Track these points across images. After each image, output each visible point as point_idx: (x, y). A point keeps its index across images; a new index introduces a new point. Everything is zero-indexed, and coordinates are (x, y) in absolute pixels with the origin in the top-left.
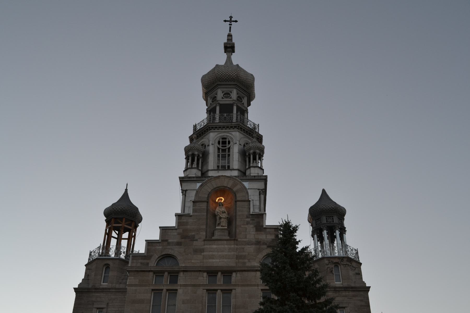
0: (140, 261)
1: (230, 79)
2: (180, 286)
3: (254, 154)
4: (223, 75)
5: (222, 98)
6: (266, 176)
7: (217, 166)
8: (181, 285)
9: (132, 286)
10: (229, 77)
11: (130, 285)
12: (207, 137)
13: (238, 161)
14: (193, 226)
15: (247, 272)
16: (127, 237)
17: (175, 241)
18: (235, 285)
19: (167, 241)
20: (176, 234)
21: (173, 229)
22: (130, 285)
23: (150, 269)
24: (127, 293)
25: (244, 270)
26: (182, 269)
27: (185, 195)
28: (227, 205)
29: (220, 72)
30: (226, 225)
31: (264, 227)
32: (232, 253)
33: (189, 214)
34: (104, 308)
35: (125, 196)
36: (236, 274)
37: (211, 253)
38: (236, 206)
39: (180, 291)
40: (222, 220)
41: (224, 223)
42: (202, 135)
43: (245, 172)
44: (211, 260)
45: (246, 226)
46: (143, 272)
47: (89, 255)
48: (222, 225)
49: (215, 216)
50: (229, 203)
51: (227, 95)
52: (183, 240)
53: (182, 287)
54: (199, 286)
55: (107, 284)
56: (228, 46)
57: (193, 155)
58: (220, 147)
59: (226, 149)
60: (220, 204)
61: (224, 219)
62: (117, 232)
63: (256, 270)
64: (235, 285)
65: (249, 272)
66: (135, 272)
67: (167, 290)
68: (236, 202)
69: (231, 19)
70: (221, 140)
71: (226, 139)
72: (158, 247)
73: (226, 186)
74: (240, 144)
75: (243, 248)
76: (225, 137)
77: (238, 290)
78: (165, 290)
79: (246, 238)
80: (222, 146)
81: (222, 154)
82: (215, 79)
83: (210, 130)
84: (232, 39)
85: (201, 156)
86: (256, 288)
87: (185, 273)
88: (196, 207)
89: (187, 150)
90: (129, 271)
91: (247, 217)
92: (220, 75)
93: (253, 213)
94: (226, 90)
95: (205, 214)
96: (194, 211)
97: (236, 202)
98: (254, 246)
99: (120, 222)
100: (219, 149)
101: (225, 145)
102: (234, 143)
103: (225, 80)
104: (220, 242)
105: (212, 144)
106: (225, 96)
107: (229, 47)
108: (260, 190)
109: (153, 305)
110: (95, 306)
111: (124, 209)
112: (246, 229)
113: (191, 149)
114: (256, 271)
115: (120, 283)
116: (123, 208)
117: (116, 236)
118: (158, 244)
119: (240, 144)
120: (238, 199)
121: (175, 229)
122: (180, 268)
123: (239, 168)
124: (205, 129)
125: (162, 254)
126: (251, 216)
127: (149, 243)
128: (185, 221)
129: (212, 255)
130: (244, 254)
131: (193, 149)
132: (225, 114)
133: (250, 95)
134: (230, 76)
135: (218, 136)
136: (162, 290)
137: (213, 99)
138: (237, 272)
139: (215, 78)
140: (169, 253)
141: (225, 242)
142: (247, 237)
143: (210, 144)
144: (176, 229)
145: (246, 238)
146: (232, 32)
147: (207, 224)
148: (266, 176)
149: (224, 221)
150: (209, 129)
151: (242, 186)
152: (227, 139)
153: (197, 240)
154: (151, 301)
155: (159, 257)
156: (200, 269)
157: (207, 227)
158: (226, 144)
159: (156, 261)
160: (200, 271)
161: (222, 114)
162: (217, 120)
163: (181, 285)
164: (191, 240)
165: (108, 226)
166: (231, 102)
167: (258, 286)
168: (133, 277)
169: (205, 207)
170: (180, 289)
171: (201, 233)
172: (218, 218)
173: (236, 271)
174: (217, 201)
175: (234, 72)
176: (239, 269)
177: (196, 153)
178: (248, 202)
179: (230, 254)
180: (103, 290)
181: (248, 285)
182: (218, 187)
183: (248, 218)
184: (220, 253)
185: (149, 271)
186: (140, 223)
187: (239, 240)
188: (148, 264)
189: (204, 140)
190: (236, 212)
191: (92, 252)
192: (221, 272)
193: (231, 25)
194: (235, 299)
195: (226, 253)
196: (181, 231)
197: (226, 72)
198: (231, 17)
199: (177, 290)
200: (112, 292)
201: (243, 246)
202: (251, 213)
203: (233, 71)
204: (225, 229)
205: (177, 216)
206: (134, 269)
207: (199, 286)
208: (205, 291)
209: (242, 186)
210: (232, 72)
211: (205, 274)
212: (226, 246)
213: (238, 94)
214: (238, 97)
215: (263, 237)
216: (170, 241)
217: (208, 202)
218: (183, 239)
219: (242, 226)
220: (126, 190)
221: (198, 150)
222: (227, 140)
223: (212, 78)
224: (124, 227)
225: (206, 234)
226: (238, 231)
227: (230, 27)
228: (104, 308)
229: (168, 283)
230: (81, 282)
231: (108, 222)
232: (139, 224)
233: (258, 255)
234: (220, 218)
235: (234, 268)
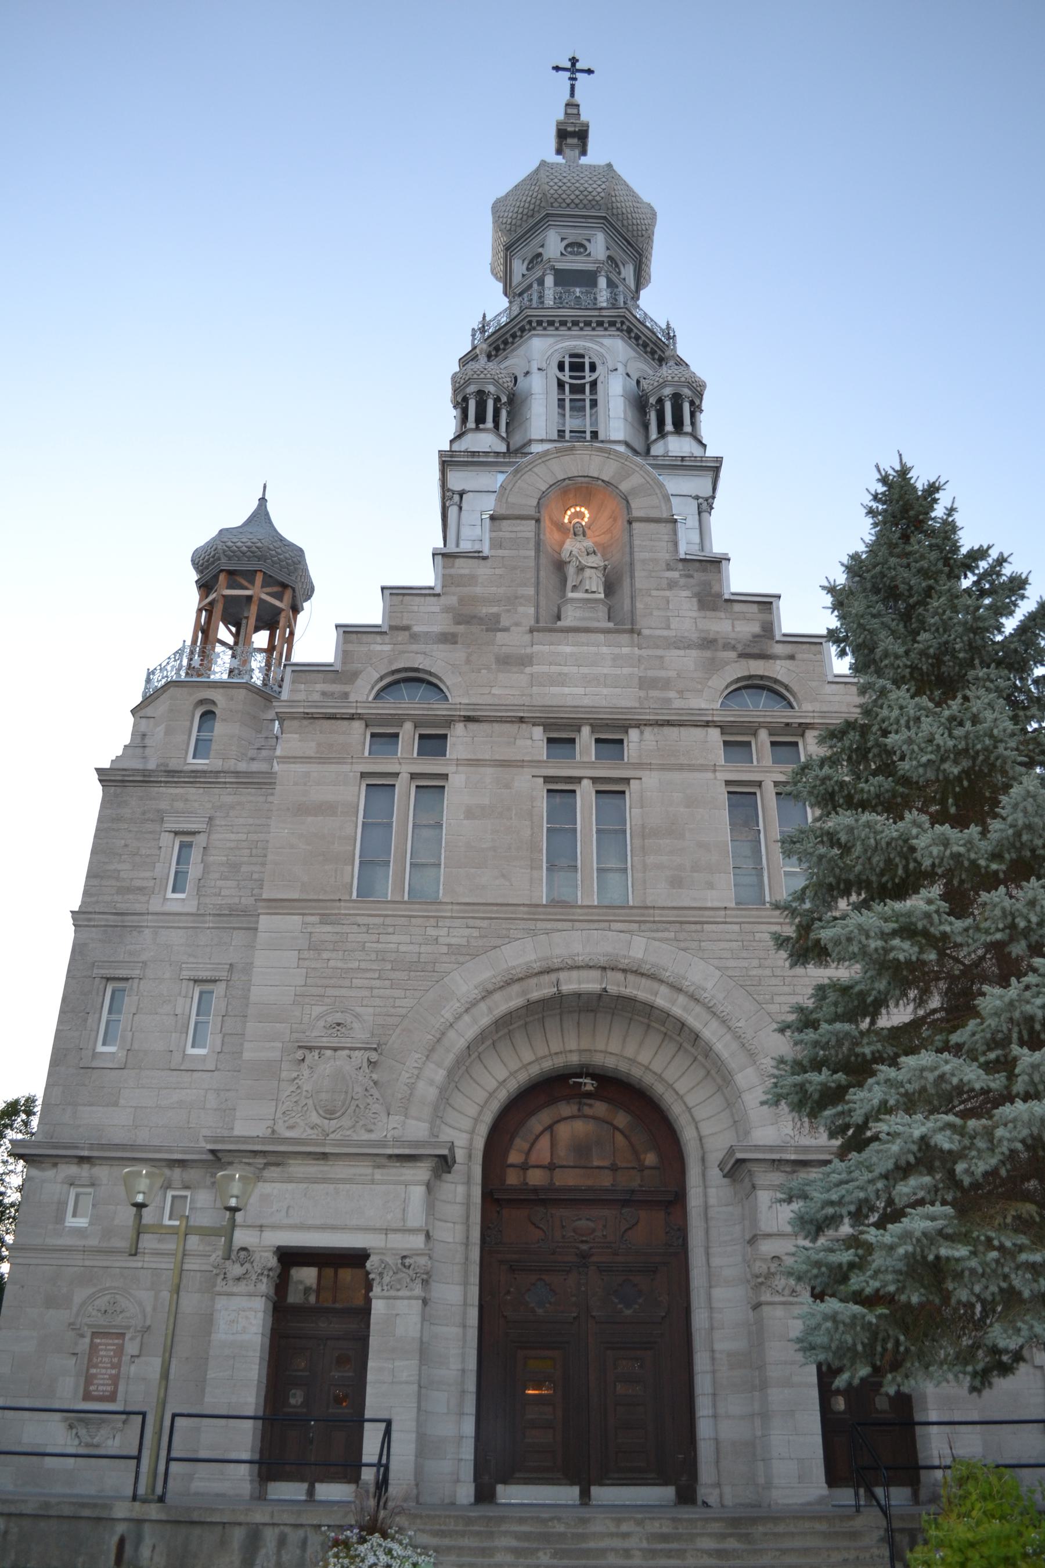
0: (319, 687)
1: (585, 202)
2: (457, 765)
4: (564, 188)
5: (562, 254)
6: (719, 460)
7: (559, 431)
8: (459, 762)
9: (294, 763)
10: (581, 197)
11: (285, 759)
12: (521, 351)
13: (625, 419)
15: (675, 729)
16: (265, 645)
17: (436, 629)
18: (640, 766)
19: (406, 628)
20: (437, 609)
21: (425, 595)
22: (285, 759)
23: (353, 711)
24: (278, 787)
25: (668, 721)
26: (462, 713)
27: (460, 508)
28: (597, 539)
29: (556, 180)
30: (601, 589)
31: (726, 597)
32: (626, 671)
33: (479, 552)
34: (199, 832)
35: (261, 514)
36: (642, 733)
37: (554, 669)
38: (631, 536)
39: (457, 780)
40: (588, 573)
41: (594, 582)
42: (504, 350)
44: (555, 690)
45: (667, 593)
46: (333, 721)
47: (144, 683)
48: (587, 587)
49: (560, 566)
50: (604, 533)
52: (461, 629)
53: (460, 768)
54: (520, 764)
55: (206, 761)
57: (481, 397)
58: (567, 379)
60: (580, 532)
61: (593, 571)
62: (233, 629)
63: (708, 722)
64: (640, 766)
65: (682, 729)
66: (305, 718)
67: (413, 776)
68: (630, 523)
69: (573, 65)
70: (567, 360)
71: (582, 356)
72: (379, 648)
73: (595, 475)
74: (628, 375)
75: (661, 657)
76: (581, 352)
77: (651, 780)
78: (404, 777)
79: (668, 628)
80: (571, 377)
81: (571, 400)
82: (538, 202)
83: (530, 330)
84: (579, 114)
85: (504, 399)
86: (710, 775)
87: (472, 726)
88: (501, 534)
89: (462, 381)
90: (281, 718)
91: (669, 568)
92: (556, 187)
93: (688, 557)
94: (574, 235)
95: (532, 553)
96: (496, 544)
97: (630, 523)
98: (694, 653)
99: (246, 583)
100: (561, 385)
102: (611, 368)
103: (568, 205)
104: (583, 637)
105: (539, 369)
106: (569, 249)
107: (573, 134)
108: (700, 501)
109: (364, 823)
110: (168, 826)
111: (259, 544)
112: (668, 602)
113: (475, 376)
114: (707, 724)
115: (253, 759)
116: (255, 540)
117: (230, 640)
118: (378, 638)
119: (628, 375)
120: (636, 513)
121: (435, 595)
122: (455, 710)
123: (628, 439)
124: (516, 329)
125: (394, 667)
126: (680, 566)
127: (348, 633)
128: (466, 571)
129: (560, 674)
130: (662, 674)
131: (482, 376)
132: (578, 290)
133: (641, 262)
134: (586, 193)
135: (556, 347)
136: (396, 775)
137: (531, 262)
138: (642, 728)
139: (540, 196)
140: (416, 666)
141: (601, 637)
142: (672, 626)
143: (534, 369)
144: (438, 595)
145: (668, 628)
146: (578, 98)
147: (538, 584)
149: (594, 577)
150: (527, 327)
151: (649, 479)
152: (587, 358)
153: (506, 630)
154: (355, 840)
155: (382, 678)
156: (522, 715)
157: (538, 593)
158: (583, 370)
159: (373, 688)
160: (521, 720)
162: (549, 302)
163: (459, 762)
164: (487, 630)
165: (207, 597)
166: (591, 267)
167: (715, 771)
168: (296, 736)
169: (532, 535)
170: (455, 773)
171: (521, 609)
172: (571, 570)
173: (639, 725)
174: (566, 521)
175: (599, 183)
176: (651, 717)
177: (491, 389)
178: (670, 526)
179: (618, 671)
180: (196, 777)
181: (681, 768)
182: (569, 478)
183: (672, 570)
184: (585, 670)
185: (352, 718)
186: (306, 600)
187: (646, 632)
188: (346, 695)
189: (514, 362)
190: (631, 553)
191: (153, 673)
192: (591, 725)
193: (575, 79)
194: (642, 807)
195: (605, 671)
196: (452, 600)
197: (573, 181)
198: (574, 61)
199: (445, 776)
200: (225, 783)
201: (659, 652)
202: (682, 556)
203: (595, 179)
204: (596, 600)
205: (439, 558)
206: (301, 710)
207: (520, 764)
208: (541, 780)
209: (649, 479)
210: (590, 182)
211: (538, 732)
212: (605, 650)
213: (608, 249)
214: (609, 257)
215: (721, 626)
216: (416, 629)
217: (538, 521)
218: (459, 623)
219: (654, 593)
220: (263, 500)
221: (496, 382)
222: (587, 361)
224: (261, 601)
225: (537, 612)
226: (639, 605)
227: (573, 87)
228: (199, 832)
229: (415, 755)
230: (120, 753)
231: (205, 586)
232: (306, 605)
233: (708, 679)
234: (581, 569)
235: (635, 713)
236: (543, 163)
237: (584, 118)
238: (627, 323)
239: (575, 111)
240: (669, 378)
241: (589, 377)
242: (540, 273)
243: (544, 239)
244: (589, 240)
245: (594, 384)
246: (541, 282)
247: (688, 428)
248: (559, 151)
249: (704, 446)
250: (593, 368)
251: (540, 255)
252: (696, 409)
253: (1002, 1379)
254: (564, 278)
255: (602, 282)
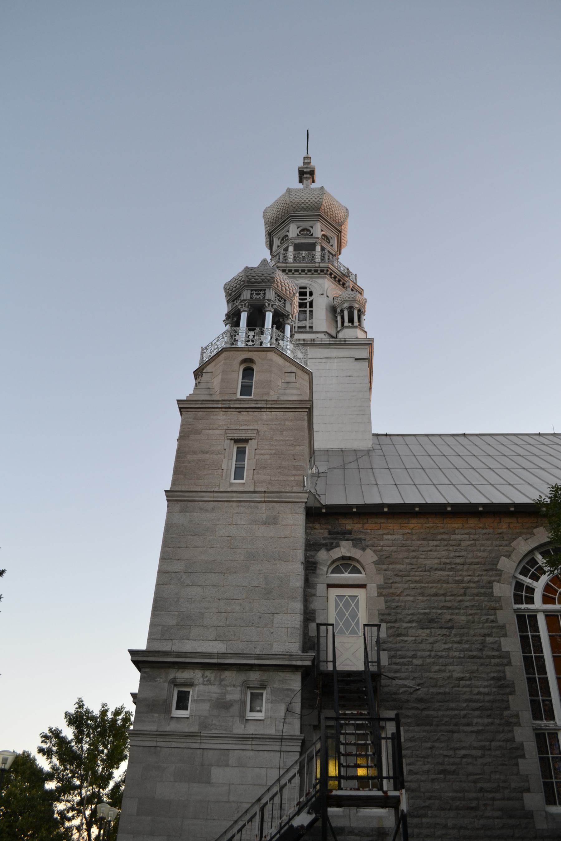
3: (351, 310)
5: (298, 235)
6: (372, 340)
14: (254, 560)
43: (319, 741)
51: (305, 233)
56: (305, 170)
59: (306, 303)
71: (306, 288)
101: (305, 309)
106: (302, 233)
132: (304, 252)
137: (282, 240)
146: (310, 154)
148: (372, 340)
158: (306, 296)
161: (298, 252)
222: (308, 291)
223: (281, 213)
236: (289, 191)
237: (313, 164)
238: (330, 271)
239: (309, 161)
240: (347, 298)
241: (309, 299)
242: (285, 246)
243: (289, 228)
244: (312, 227)
245: (311, 305)
246: (286, 250)
247: (356, 323)
248: (301, 181)
249: (366, 332)
250: (311, 294)
251: (287, 236)
252: (361, 313)
253: (255, 263)
254: (298, 247)
255: (318, 248)
